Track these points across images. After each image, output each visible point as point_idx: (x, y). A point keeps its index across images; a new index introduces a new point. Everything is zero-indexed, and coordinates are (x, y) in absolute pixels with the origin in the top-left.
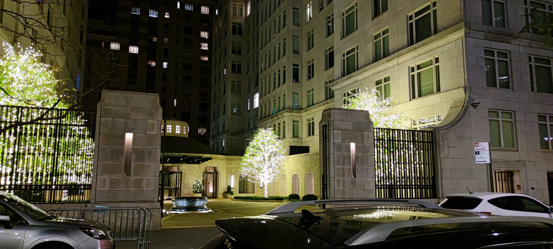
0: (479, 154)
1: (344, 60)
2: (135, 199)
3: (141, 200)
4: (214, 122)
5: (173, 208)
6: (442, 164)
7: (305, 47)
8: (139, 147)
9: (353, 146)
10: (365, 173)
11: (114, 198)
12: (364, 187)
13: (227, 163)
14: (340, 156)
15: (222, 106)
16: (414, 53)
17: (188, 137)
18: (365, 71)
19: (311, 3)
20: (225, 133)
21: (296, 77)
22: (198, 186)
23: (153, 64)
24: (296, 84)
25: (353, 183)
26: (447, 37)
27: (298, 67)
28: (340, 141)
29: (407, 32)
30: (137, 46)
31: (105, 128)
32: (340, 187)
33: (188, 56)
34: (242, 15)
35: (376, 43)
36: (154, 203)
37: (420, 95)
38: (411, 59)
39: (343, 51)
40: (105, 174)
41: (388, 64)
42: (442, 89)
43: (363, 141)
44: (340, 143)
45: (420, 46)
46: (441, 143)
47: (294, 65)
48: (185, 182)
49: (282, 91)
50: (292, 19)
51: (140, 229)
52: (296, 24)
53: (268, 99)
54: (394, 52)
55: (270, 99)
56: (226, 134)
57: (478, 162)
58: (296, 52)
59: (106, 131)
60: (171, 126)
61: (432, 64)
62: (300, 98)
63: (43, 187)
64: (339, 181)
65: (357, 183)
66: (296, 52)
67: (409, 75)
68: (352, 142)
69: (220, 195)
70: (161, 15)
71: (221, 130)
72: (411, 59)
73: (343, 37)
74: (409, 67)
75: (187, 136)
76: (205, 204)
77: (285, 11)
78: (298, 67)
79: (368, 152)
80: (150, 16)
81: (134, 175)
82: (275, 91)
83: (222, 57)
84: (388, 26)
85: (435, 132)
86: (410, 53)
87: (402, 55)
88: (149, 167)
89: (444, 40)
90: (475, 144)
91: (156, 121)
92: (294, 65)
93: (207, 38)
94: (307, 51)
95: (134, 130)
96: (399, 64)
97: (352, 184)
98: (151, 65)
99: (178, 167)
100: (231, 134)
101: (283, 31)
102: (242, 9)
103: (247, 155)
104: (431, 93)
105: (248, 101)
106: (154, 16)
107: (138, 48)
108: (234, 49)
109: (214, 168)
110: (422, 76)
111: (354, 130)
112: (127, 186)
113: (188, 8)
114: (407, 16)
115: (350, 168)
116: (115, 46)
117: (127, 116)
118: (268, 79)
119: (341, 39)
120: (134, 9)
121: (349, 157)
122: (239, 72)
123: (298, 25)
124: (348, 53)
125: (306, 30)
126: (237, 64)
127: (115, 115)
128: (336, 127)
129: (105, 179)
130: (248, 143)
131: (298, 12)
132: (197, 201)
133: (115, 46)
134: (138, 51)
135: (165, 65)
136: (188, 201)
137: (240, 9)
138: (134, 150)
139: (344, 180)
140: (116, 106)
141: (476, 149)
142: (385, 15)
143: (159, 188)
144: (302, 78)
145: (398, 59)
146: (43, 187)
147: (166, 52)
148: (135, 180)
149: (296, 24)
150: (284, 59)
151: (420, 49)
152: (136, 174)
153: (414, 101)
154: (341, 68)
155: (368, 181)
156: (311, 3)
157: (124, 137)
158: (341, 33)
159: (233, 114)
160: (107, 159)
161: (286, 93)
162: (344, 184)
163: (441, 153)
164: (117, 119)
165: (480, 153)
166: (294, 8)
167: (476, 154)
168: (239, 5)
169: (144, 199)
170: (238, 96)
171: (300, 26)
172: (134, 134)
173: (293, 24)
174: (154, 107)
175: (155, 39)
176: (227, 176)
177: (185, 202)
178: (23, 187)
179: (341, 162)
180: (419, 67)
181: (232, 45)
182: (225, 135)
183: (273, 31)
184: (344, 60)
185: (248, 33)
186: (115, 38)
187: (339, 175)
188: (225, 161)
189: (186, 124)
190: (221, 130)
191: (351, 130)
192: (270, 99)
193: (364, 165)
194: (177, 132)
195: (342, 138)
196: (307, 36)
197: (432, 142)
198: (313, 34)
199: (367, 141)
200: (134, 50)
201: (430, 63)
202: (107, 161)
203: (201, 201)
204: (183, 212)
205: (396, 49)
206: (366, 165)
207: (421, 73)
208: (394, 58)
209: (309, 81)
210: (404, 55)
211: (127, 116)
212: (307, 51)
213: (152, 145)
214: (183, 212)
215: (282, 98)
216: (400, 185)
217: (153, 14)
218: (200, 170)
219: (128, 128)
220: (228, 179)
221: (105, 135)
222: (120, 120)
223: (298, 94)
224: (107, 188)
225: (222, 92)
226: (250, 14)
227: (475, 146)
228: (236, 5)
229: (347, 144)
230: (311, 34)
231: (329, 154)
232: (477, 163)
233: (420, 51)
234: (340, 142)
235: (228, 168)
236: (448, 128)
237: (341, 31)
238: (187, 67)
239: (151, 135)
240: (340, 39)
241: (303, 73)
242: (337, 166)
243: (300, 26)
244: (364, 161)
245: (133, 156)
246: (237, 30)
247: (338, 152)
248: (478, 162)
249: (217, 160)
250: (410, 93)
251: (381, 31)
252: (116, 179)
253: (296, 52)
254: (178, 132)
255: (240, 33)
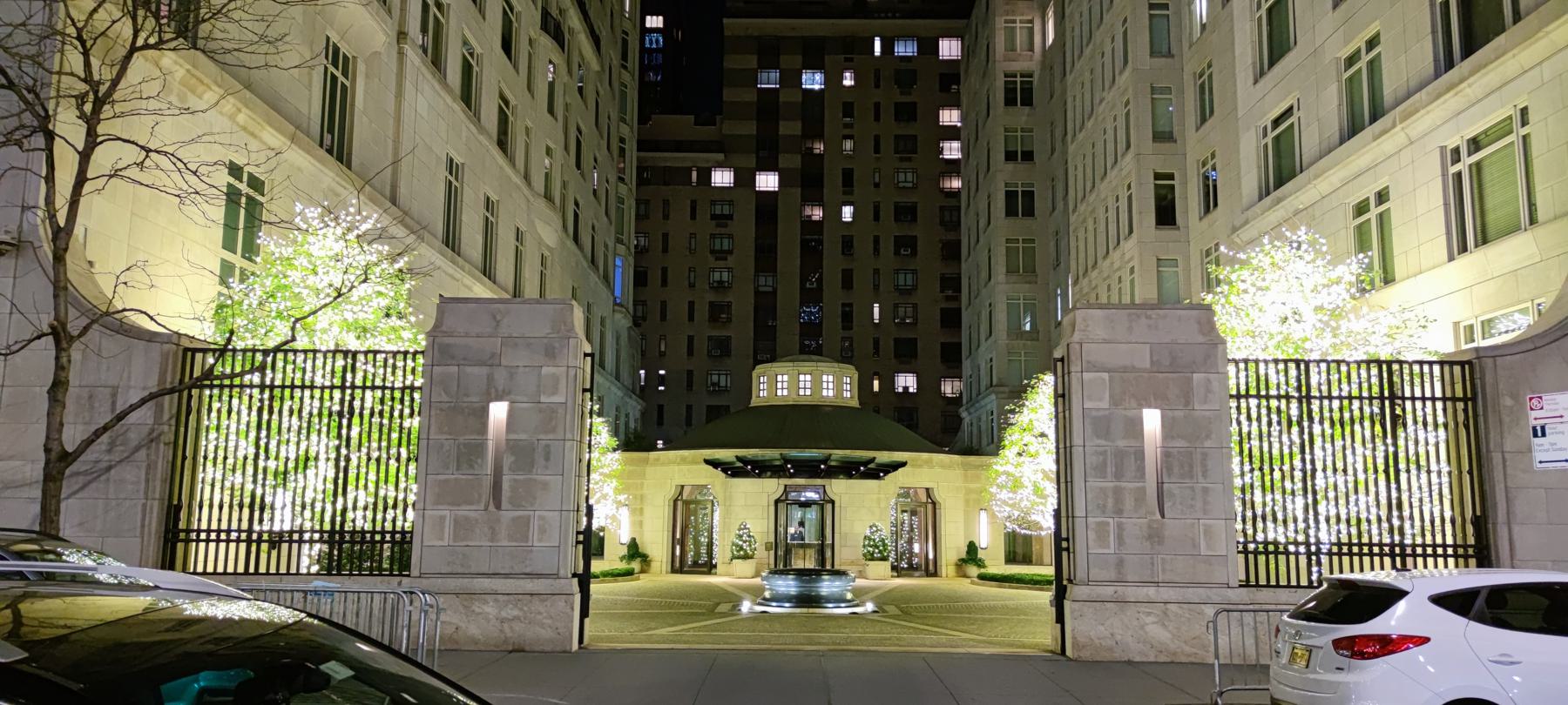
0: (1544, 435)
1: (1266, 146)
2: (512, 568)
3: (528, 570)
4: (969, 361)
5: (765, 599)
6: (1509, 471)
7: (1191, 117)
8: (523, 436)
9: (1152, 420)
10: (1199, 504)
11: (462, 566)
12: (1195, 545)
13: (966, 476)
14: (1106, 451)
16: (1451, 102)
17: (858, 406)
18: (1317, 177)
20: (993, 392)
21: (1166, 215)
22: (874, 540)
23: (817, 214)
24: (1167, 233)
25: (1154, 536)
26: (1548, 33)
27: (1173, 179)
28: (1105, 404)
29: (1434, 32)
30: (774, 171)
31: (443, 393)
32: (1109, 547)
33: (906, 182)
34: (1031, 49)
35: (1350, 79)
36: (558, 581)
37: (1484, 239)
38: (1446, 122)
39: (1261, 119)
40: (442, 504)
41: (1378, 145)
42: (1541, 214)
43: (1187, 403)
44: (1107, 412)
45: (1466, 74)
46: (1508, 402)
47: (1157, 176)
48: (843, 528)
49: (1127, 257)
50: (1148, 39)
51: (402, 642)
52: (1161, 48)
53: (1093, 285)
54: (1398, 103)
55: (1096, 286)
56: (997, 393)
57: (1541, 462)
59: (445, 398)
60: (808, 377)
61: (1512, 132)
62: (1181, 273)
64: (1102, 529)
65: (1167, 533)
66: (1163, 136)
67: (1444, 174)
68: (1150, 407)
70: (833, 80)
71: (985, 382)
72: (1446, 122)
74: (1443, 149)
75: (855, 403)
76: (848, 590)
78: (1173, 179)
79: (1208, 437)
81: (510, 507)
82: (1108, 261)
83: (981, 177)
84: (1377, 23)
85: (1480, 362)
86: (1442, 100)
87: (1417, 111)
88: (545, 485)
89: (1537, 45)
90: (1531, 399)
91: (564, 369)
92: (1157, 176)
93: (959, 124)
94: (1197, 129)
95: (509, 393)
96: (1412, 143)
97: (1150, 537)
98: (810, 216)
100: (1011, 392)
101: (1124, 79)
102: (1031, 30)
103: (1009, 453)
104: (1513, 229)
105: (1056, 295)
106: (817, 87)
107: (777, 177)
108: (1011, 149)
109: (927, 489)
110: (1488, 175)
111: (1155, 369)
112: (493, 536)
113: (904, 49)
115: (1143, 490)
116: (722, 178)
117: (492, 361)
118: (1091, 228)
119: (1256, 82)
120: (765, 75)
121: (1140, 454)
122: (1029, 212)
123: (1169, 55)
124: (1276, 122)
125: (1191, 66)
126: (1020, 189)
127: (464, 359)
128: (1088, 362)
129: (443, 518)
130: (1007, 419)
132: (824, 580)
133: (722, 178)
134: (777, 185)
135: (847, 213)
137: (1025, 32)
138: (513, 446)
139: (1120, 527)
140: (467, 335)
141: (1534, 418)
143: (578, 542)
144: (1186, 212)
145: (1408, 126)
147: (848, 177)
148: (515, 519)
149: (1161, 48)
151: (1470, 86)
152: (516, 505)
153: (1463, 261)
154: (1259, 171)
155: (1208, 531)
157: (484, 412)
158: (1254, 63)
159: (1016, 332)
160: (448, 468)
163: (1506, 435)
164: (469, 369)
165: (1547, 431)
167: (1535, 435)
168: (1021, 22)
169: (539, 569)
170: (1026, 283)
171: (1173, 56)
172: (512, 402)
174: (558, 332)
175: (819, 147)
176: (966, 513)
177: (791, 582)
179: (1110, 469)
180: (1475, 144)
181: (1006, 136)
182: (993, 397)
184: (1266, 146)
185: (1052, 97)
186: (721, 156)
187: (1103, 509)
188: (959, 472)
189: (754, 374)
190: (985, 382)
191: (1144, 370)
192: (1096, 286)
193: (1192, 477)
194: (825, 393)
195: (1111, 397)
196: (1339, 75)
197: (1474, 399)
198: (1210, 76)
199: (1205, 402)
200: (768, 182)
201: (1503, 128)
202: (447, 472)
203: (834, 581)
205: (1402, 92)
206: (1201, 479)
207: (1485, 163)
208: (1394, 126)
209: (1205, 221)
210: (1422, 112)
211: (492, 361)
212: (1197, 129)
213: (554, 430)
214: (786, 609)
216: (1392, 546)
218: (882, 496)
219: (497, 391)
220: (970, 522)
221: (441, 410)
222: (476, 370)
223: (1174, 262)
224: (446, 540)
225: (984, 274)
226: (1054, 41)
227: (1532, 409)
228: (1014, 21)
229: (1131, 413)
231: (1071, 447)
232: (1539, 465)
233: (1468, 90)
234: (1107, 406)
235: (969, 491)
236: (1535, 348)
237: (1254, 57)
239: (552, 406)
240: (1251, 80)
241: (1189, 199)
242: (1094, 483)
243: (1173, 56)
244: (1191, 466)
245: (508, 461)
247: (1098, 437)
248: (1541, 462)
249: (932, 467)
250: (1448, 233)
251: (1360, 42)
252: (467, 518)
253: (1163, 136)
254: (828, 392)
255: (1028, 101)
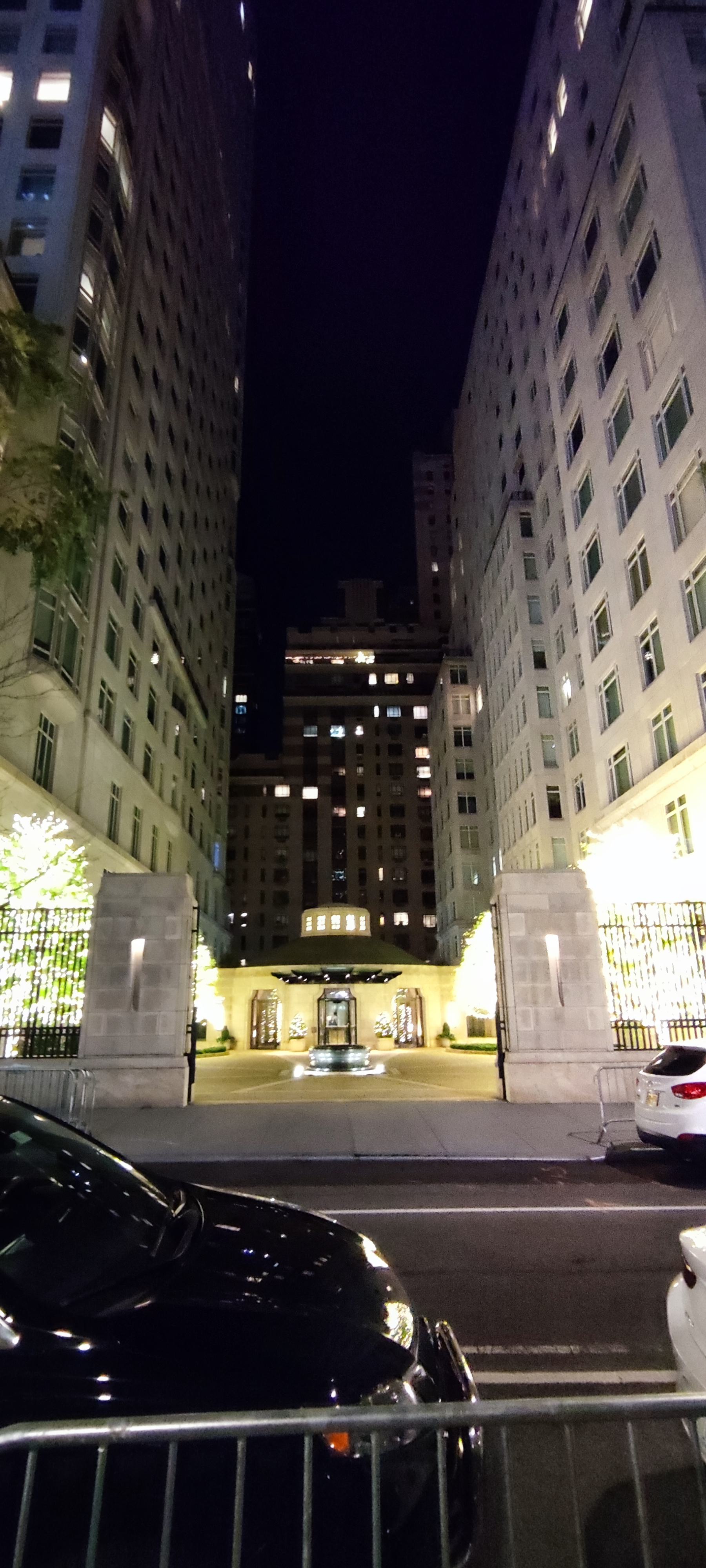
15: (449, 875)
19: (567, 675)
21: (555, 811)
23: (342, 812)
25: (558, 1018)
34: (469, 712)
47: (549, 788)
52: (545, 712)
54: (685, 746)
58: (551, 764)
63: (58, 1031)
69: (430, 1042)
73: (604, 728)
75: (368, 934)
77: (523, 697)
80: (305, 736)
92: (549, 788)
98: (337, 814)
99: (349, 989)
102: (468, 703)
105: (492, 862)
114: (697, 675)
116: (282, 791)
118: (511, 820)
119: (602, 733)
121: (546, 964)
122: (473, 810)
123: (551, 716)
125: (564, 722)
131: (548, 694)
133: (282, 791)
136: (335, 1053)
139: (537, 1014)
142: (663, 675)
146: (58, 1031)
150: (530, 780)
156: (567, 675)
161: (539, 841)
162: (537, 1021)
166: (538, 688)
173: (540, 715)
175: (343, 772)
178: (37, 1031)
183: (510, 734)
190: (450, 917)
200: (310, 793)
204: (325, 1072)
208: (684, 759)
214: (325, 1072)
215: (534, 850)
217: (338, 732)
230: (663, 723)
238: (398, 811)
241: (568, 802)
242: (522, 985)
245: (143, 979)
246: (463, 739)
254: (350, 927)
255: (469, 743)
